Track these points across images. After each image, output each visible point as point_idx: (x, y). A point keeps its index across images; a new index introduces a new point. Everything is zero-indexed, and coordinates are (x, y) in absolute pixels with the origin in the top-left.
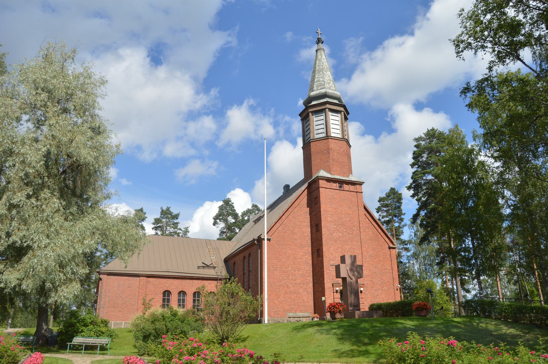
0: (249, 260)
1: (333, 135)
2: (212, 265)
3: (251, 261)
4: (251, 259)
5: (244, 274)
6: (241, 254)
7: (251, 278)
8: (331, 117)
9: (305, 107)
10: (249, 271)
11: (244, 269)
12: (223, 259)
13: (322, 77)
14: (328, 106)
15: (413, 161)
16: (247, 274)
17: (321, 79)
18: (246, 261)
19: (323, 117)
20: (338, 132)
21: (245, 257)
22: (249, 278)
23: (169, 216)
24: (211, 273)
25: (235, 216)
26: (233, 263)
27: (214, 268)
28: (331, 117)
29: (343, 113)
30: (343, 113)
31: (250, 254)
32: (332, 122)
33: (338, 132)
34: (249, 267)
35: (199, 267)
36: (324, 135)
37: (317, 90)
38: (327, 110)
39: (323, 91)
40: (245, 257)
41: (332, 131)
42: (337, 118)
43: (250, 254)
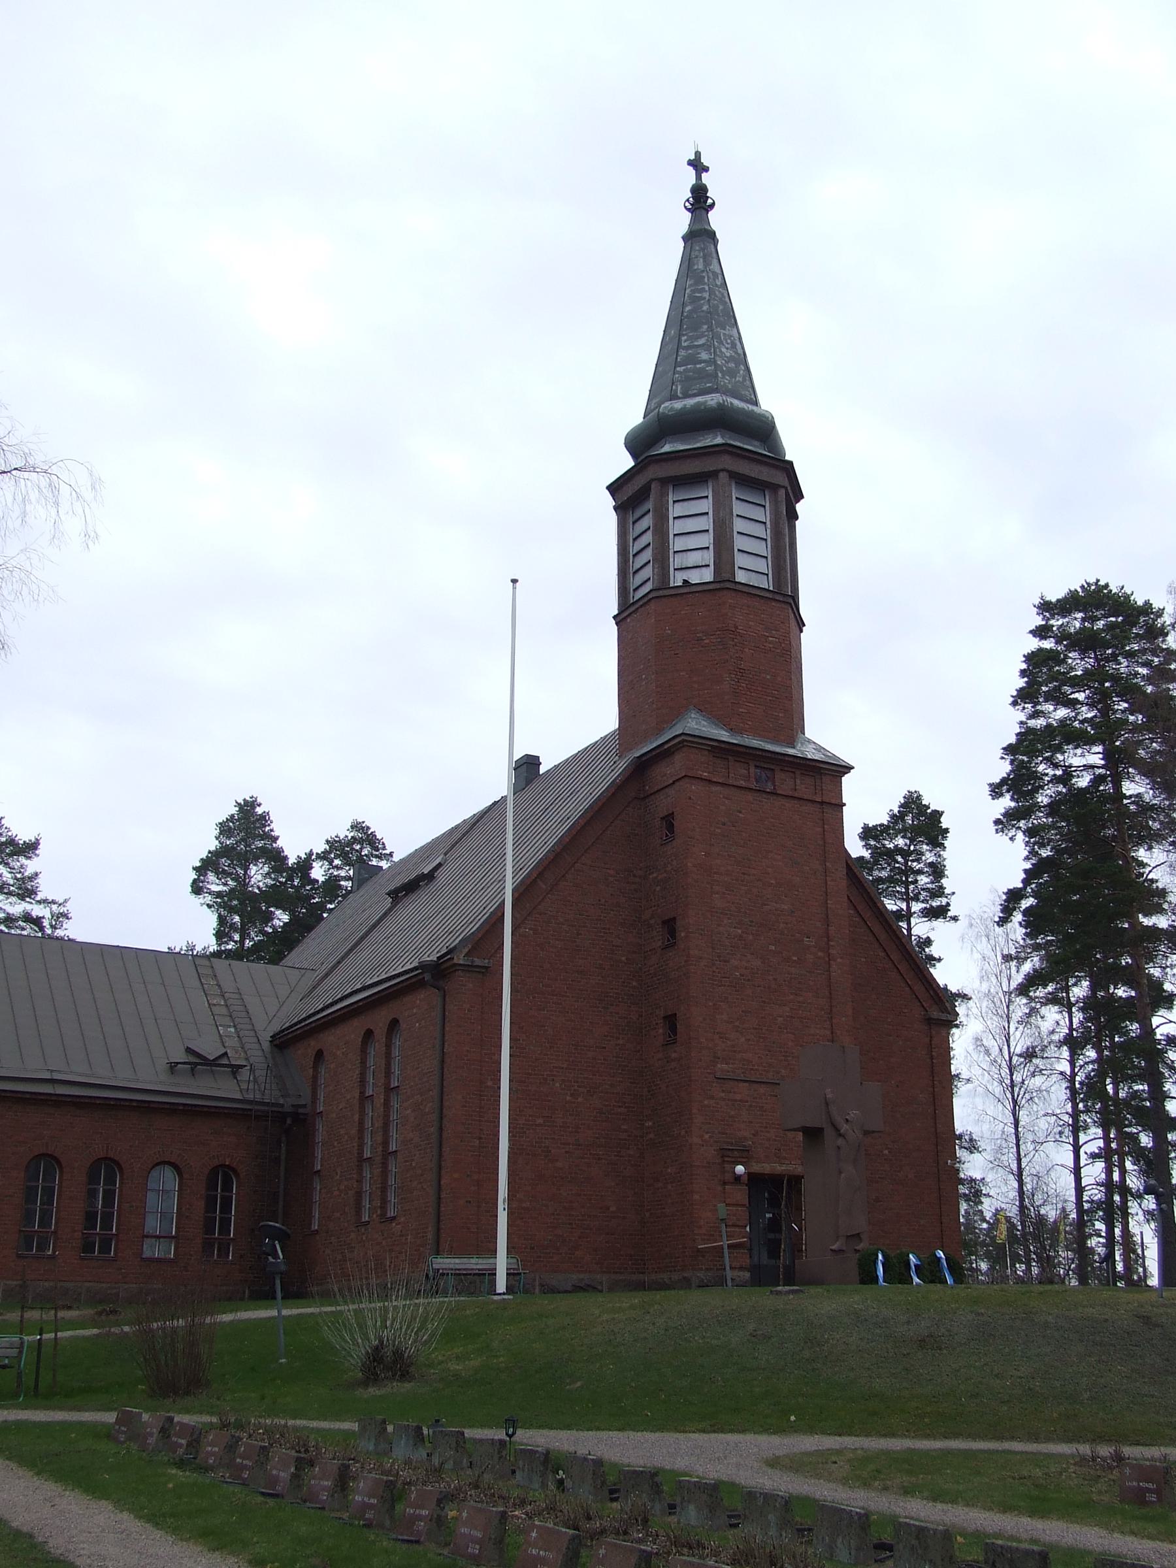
0: (389, 1046)
1: (741, 577)
2: (225, 1061)
3: (396, 1052)
4: (397, 1042)
5: (364, 1098)
6: (356, 1022)
7: (393, 1116)
8: (738, 508)
9: (628, 463)
10: (389, 1090)
11: (363, 1082)
12: (266, 1037)
13: (706, 347)
14: (727, 462)
15: (1021, 683)
16: (379, 1101)
17: (704, 356)
18: (375, 1051)
19: (706, 506)
20: (761, 565)
21: (369, 1034)
22: (386, 1116)
23: (1146, 1140)
24: (224, 1089)
25: (276, 858)
26: (311, 1053)
27: (235, 1069)
28: (738, 508)
29: (782, 492)
30: (782, 492)
31: (394, 1023)
32: (739, 525)
33: (761, 565)
34: (388, 1073)
35: (173, 1067)
36: (707, 575)
37: (686, 396)
38: (723, 476)
39: (712, 400)
40: (369, 1034)
41: (740, 560)
42: (758, 514)
43: (394, 1023)
